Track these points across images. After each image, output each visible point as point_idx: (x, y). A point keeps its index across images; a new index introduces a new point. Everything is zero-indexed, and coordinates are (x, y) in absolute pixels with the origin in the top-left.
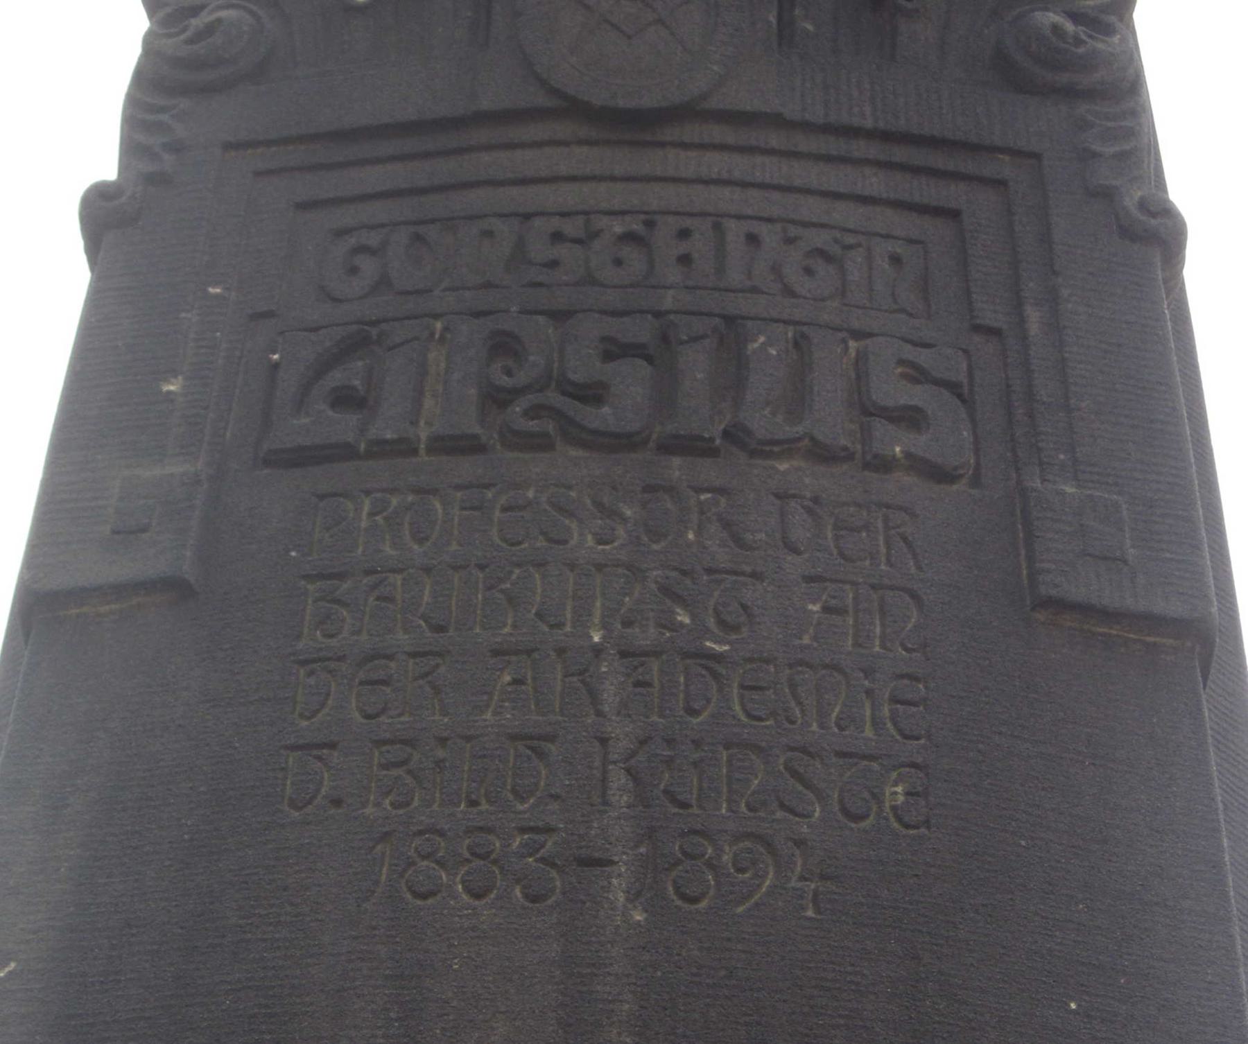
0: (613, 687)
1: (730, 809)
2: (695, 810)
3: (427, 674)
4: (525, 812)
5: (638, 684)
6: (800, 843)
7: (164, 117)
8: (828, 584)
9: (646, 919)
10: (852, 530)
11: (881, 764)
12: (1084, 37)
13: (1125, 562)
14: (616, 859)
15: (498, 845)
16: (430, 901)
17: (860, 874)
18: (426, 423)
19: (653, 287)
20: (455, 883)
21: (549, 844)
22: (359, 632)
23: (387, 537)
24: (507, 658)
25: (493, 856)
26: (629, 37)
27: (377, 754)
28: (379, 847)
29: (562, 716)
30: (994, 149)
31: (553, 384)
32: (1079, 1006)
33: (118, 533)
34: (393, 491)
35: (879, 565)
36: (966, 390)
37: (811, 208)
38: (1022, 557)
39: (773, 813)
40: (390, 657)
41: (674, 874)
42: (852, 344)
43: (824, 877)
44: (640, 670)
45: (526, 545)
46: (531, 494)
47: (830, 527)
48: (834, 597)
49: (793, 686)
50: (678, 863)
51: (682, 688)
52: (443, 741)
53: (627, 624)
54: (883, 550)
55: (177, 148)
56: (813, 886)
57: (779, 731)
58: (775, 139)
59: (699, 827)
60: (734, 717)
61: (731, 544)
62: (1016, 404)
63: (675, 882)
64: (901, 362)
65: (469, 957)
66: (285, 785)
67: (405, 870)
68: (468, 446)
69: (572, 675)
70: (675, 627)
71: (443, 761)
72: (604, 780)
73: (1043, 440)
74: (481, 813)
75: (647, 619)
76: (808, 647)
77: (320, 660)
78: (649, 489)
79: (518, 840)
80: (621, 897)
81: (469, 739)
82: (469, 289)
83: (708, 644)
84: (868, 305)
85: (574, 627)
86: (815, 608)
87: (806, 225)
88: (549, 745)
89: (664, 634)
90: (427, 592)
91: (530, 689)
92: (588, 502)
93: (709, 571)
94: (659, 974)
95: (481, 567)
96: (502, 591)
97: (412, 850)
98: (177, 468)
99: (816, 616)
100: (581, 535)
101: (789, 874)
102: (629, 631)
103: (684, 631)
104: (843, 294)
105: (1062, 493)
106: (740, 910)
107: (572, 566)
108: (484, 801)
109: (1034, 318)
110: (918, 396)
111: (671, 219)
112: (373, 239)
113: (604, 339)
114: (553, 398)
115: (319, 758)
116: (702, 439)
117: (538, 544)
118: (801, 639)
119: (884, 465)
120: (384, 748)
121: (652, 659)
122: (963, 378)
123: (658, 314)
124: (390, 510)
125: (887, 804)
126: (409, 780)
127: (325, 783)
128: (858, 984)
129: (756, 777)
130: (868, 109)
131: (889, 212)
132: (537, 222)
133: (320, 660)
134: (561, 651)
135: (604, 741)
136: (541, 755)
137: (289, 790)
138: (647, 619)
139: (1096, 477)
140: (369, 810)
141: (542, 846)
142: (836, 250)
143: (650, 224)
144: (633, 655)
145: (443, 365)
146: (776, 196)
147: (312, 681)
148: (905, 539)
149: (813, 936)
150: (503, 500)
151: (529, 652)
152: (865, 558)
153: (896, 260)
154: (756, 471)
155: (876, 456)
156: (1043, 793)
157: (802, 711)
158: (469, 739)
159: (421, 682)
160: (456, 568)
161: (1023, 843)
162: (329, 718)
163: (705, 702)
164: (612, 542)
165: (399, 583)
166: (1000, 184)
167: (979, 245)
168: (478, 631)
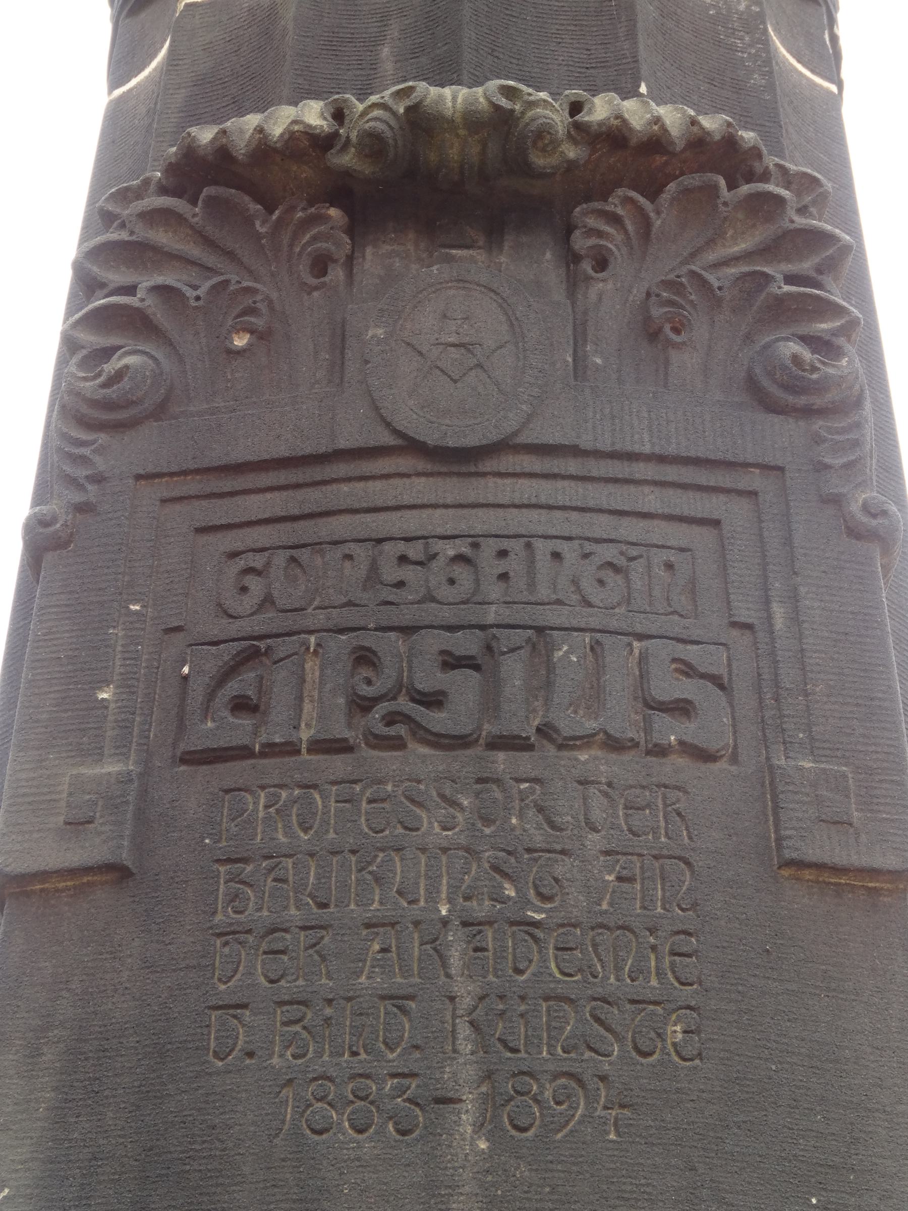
0: (457, 954)
1: (549, 1053)
2: (523, 1055)
3: (314, 945)
4: (394, 1061)
5: (476, 950)
6: (603, 1078)
7: (86, 451)
8: (620, 857)
9: (488, 1147)
10: (638, 809)
11: (663, 1008)
12: (818, 365)
13: (851, 825)
14: (464, 1098)
15: (374, 1088)
16: (324, 1136)
17: (649, 1102)
18: (306, 725)
19: (480, 603)
20: (343, 1121)
21: (413, 1086)
22: (259, 909)
23: (280, 826)
24: (376, 930)
25: (371, 1098)
26: (455, 381)
27: (279, 1012)
28: (284, 1091)
29: (420, 978)
30: (746, 465)
31: (404, 690)
32: (818, 1201)
33: (70, 824)
34: (281, 786)
35: (660, 838)
36: (726, 680)
37: (602, 525)
38: (771, 822)
39: (582, 1054)
40: (286, 930)
41: (508, 1108)
42: (636, 644)
43: (622, 1106)
44: (478, 938)
45: (387, 832)
46: (389, 788)
47: (621, 806)
48: (624, 868)
49: (595, 946)
50: (511, 1099)
51: (510, 950)
52: (330, 1002)
53: (467, 898)
54: (662, 824)
55: (98, 479)
56: (614, 1113)
57: (585, 985)
58: (572, 466)
59: (525, 1069)
60: (550, 975)
61: (545, 826)
62: (765, 690)
63: (509, 1116)
64: (674, 660)
65: (355, 1183)
66: (209, 1039)
67: (304, 1111)
68: (340, 747)
69: (426, 943)
70: (504, 900)
71: (330, 1018)
72: (453, 1031)
73: (786, 722)
74: (360, 1062)
75: (483, 894)
76: (606, 912)
77: (234, 933)
78: (480, 781)
79: (389, 1083)
80: (469, 1129)
81: (349, 999)
82: (335, 607)
83: (529, 913)
84: (648, 609)
85: (426, 901)
86: (610, 878)
87: (598, 541)
88: (410, 1003)
89: (495, 906)
90: (312, 874)
91: (394, 955)
92: (434, 794)
93: (529, 850)
94: (499, 1192)
95: (353, 852)
96: (370, 873)
97: (310, 1094)
98: (112, 768)
99: (612, 884)
100: (430, 823)
101: (595, 1105)
102: (468, 904)
103: (511, 903)
104: (629, 603)
105: (800, 769)
106: (559, 1136)
107: (423, 850)
108: (362, 1051)
109: (779, 612)
110: (686, 689)
111: (491, 541)
112: (258, 561)
113: (443, 652)
114: (404, 704)
115: (235, 1017)
116: (520, 737)
117: (397, 832)
118: (600, 905)
119: (660, 751)
120: (285, 1008)
121: (487, 927)
122: (723, 671)
123: (483, 628)
124: (281, 803)
125: (669, 1042)
126: (305, 1034)
127: (241, 1037)
128: (649, 1194)
129: (569, 1024)
130: (646, 437)
131: (663, 524)
132: (387, 546)
133: (234, 933)
134: (416, 924)
135: (452, 999)
136: (404, 1011)
137: (213, 1044)
138: (483, 894)
139: (828, 752)
140: (275, 1061)
141: (409, 1088)
142: (621, 561)
143: (475, 546)
144: (472, 924)
145: (317, 674)
146: (574, 515)
147: (226, 950)
148: (679, 814)
149: (614, 1156)
150: (368, 794)
151: (393, 925)
152: (649, 833)
153: (669, 566)
154: (562, 762)
155: (656, 745)
156: (788, 1024)
157: (603, 967)
158: (349, 999)
159: (311, 951)
160: (334, 853)
161: (774, 1067)
162: (241, 983)
163: (527, 963)
164: (453, 828)
165: (290, 866)
166: (752, 494)
167: (736, 551)
168: (352, 907)
